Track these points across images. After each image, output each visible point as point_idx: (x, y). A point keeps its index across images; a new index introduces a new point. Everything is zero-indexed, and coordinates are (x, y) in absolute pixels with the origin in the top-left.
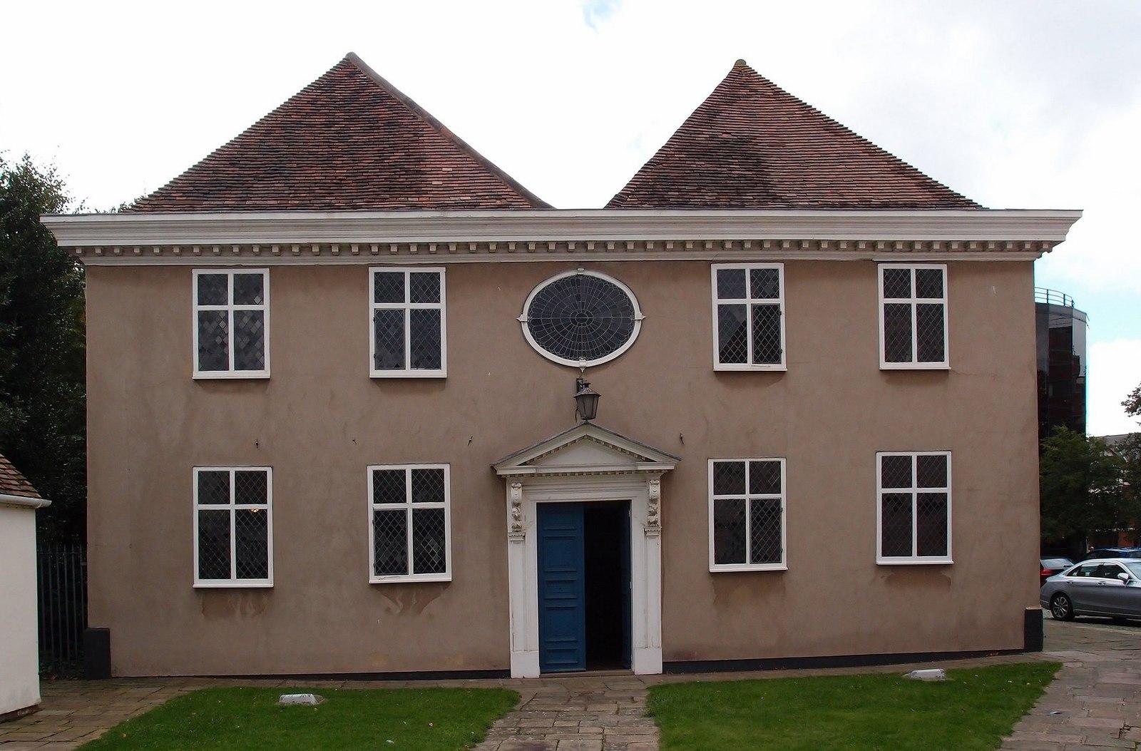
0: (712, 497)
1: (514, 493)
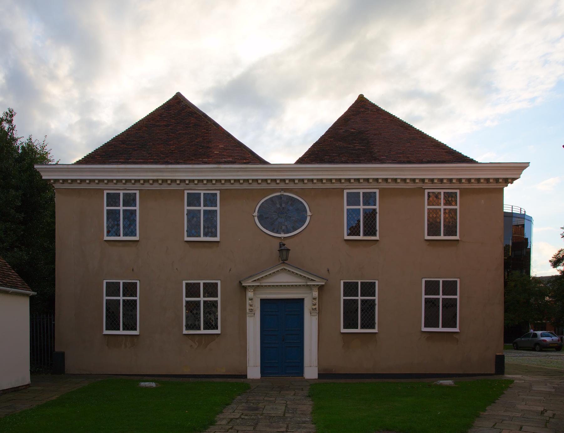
1: (250, 294)
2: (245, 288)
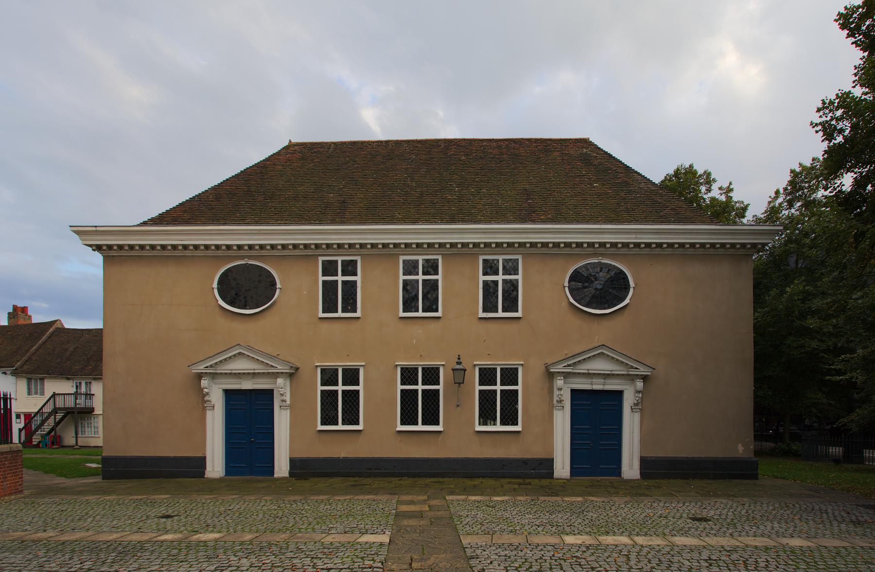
1: (559, 382)
2: (551, 376)
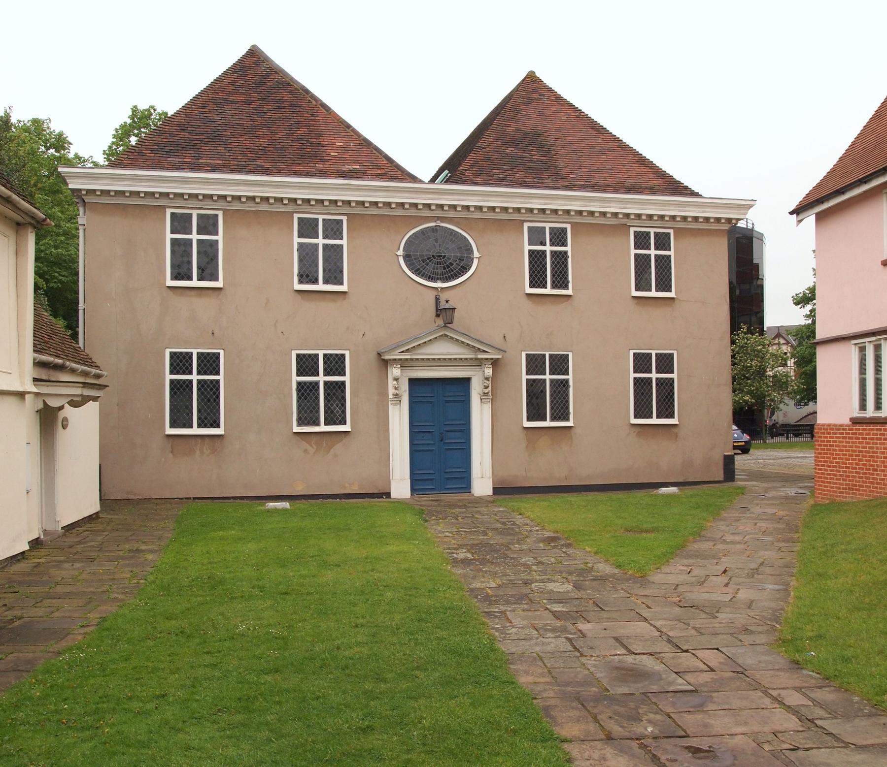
0: (525, 377)
2: (385, 363)
